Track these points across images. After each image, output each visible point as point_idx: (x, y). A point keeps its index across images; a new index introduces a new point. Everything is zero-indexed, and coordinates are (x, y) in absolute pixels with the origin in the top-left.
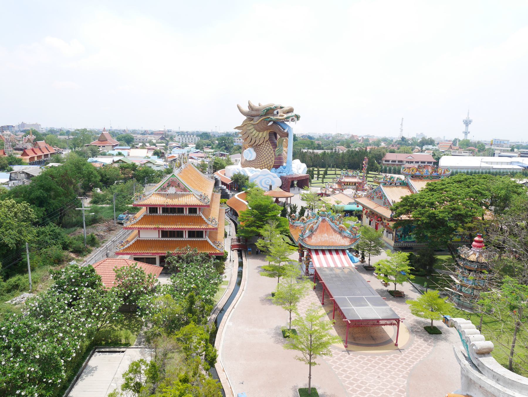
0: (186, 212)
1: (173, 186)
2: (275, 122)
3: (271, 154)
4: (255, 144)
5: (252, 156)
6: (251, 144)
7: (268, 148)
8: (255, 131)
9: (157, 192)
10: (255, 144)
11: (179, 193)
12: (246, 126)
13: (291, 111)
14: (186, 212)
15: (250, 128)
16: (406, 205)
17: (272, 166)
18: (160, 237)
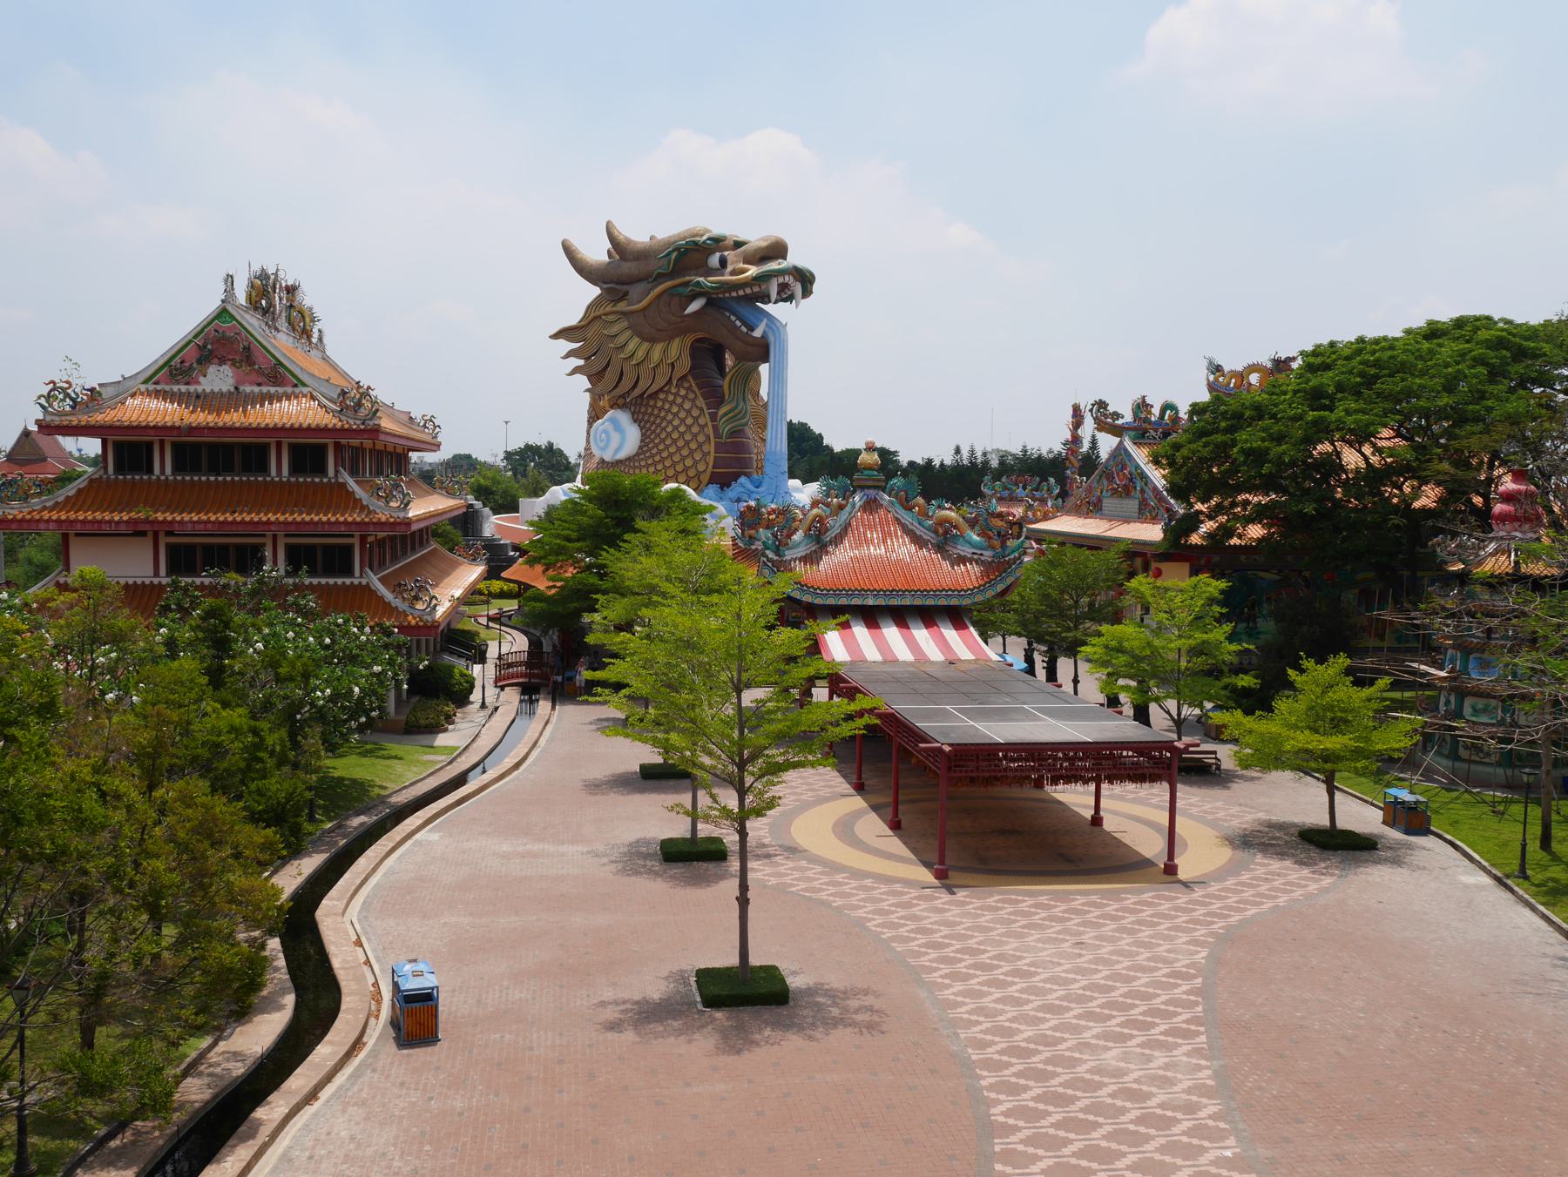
0: (280, 469)
1: (222, 361)
2: (717, 301)
3: (702, 427)
4: (637, 392)
5: (623, 440)
6: (618, 392)
7: (687, 405)
8: (636, 340)
9: (151, 387)
10: (637, 392)
11: (248, 389)
12: (598, 324)
13: (777, 250)
14: (280, 469)
15: (615, 329)
16: (1216, 431)
17: (705, 478)
18: (163, 571)
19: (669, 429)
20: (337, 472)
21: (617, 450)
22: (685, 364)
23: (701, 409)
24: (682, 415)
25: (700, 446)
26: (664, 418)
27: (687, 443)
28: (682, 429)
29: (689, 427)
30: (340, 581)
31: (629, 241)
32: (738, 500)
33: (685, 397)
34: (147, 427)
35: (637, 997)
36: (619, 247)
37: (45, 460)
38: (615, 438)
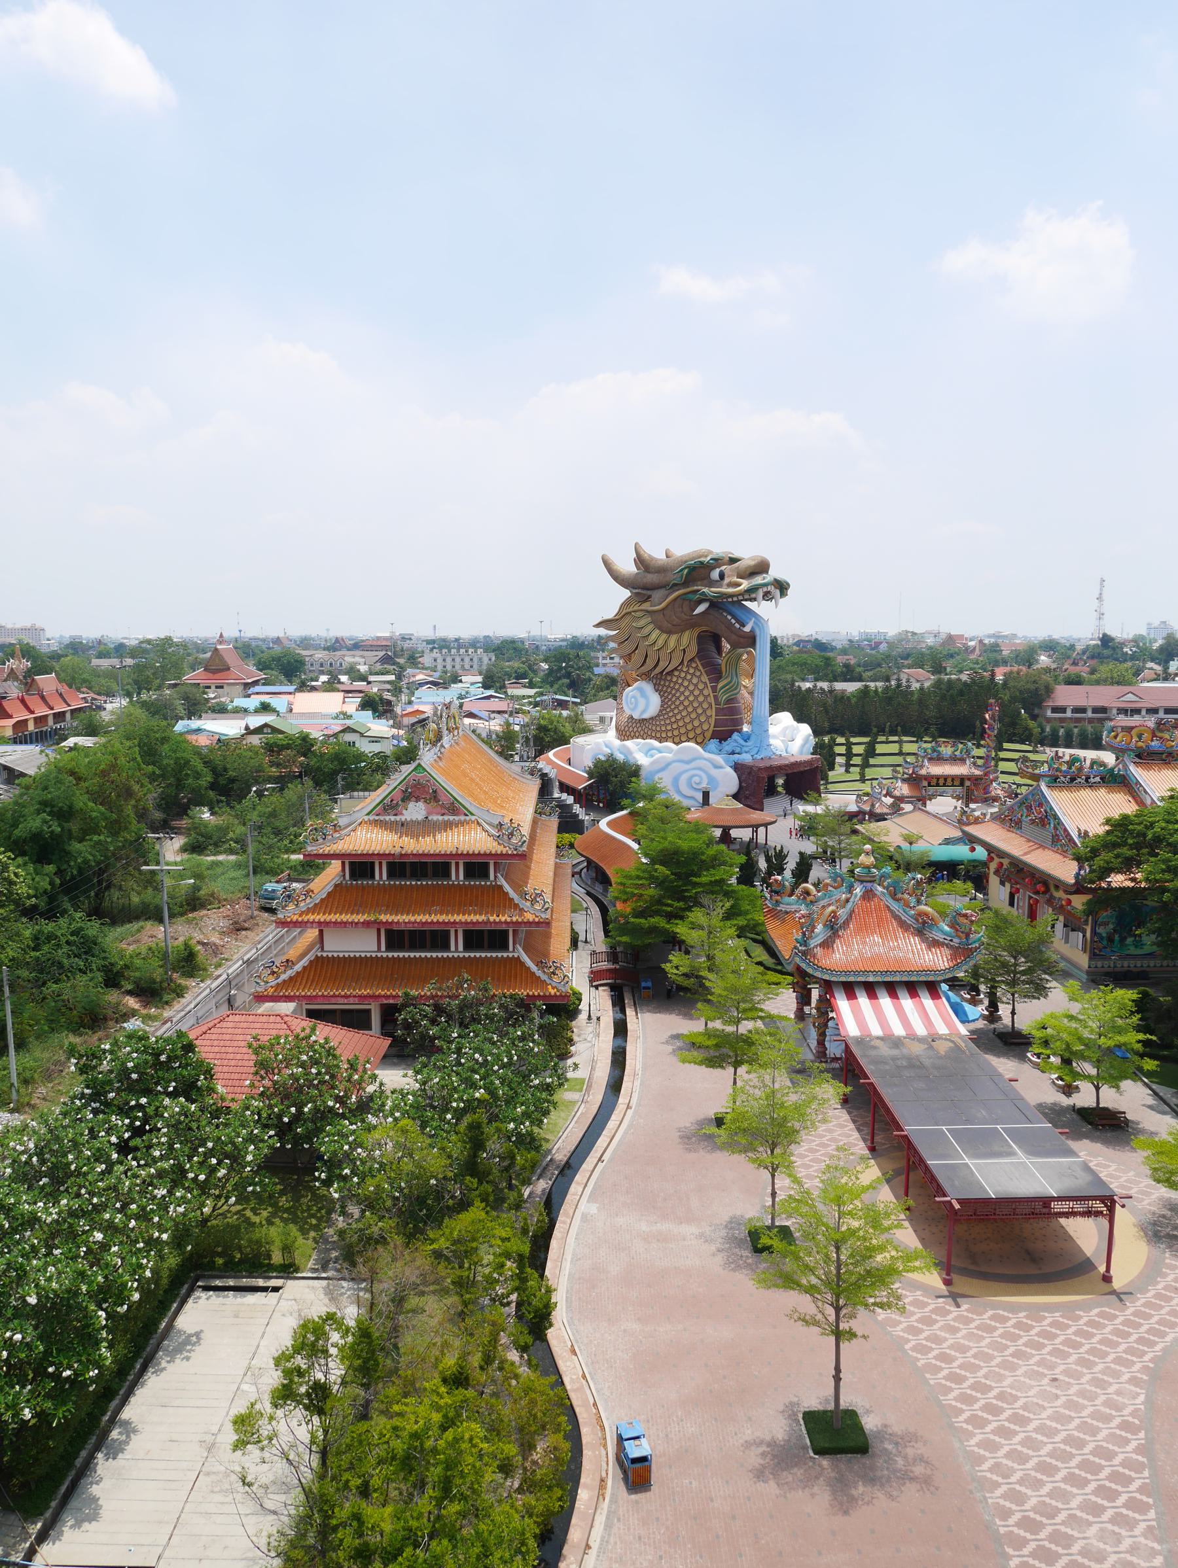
0: (458, 876)
1: (418, 799)
2: (717, 605)
4: (658, 670)
5: (647, 706)
6: (645, 669)
8: (657, 632)
9: (372, 817)
10: (658, 670)
11: (435, 818)
12: (627, 619)
13: (762, 567)
14: (458, 876)
15: (642, 623)
17: (708, 734)
18: (383, 948)
19: (682, 698)
20: (496, 877)
21: (644, 711)
22: (693, 650)
23: (705, 684)
24: (691, 687)
25: (704, 711)
26: (678, 690)
27: (695, 709)
28: (691, 698)
29: (696, 697)
30: (500, 955)
31: (652, 558)
32: (733, 753)
33: (693, 675)
34: (373, 854)
35: (768, 1438)
36: (641, 561)
37: (229, 669)
38: (642, 703)
